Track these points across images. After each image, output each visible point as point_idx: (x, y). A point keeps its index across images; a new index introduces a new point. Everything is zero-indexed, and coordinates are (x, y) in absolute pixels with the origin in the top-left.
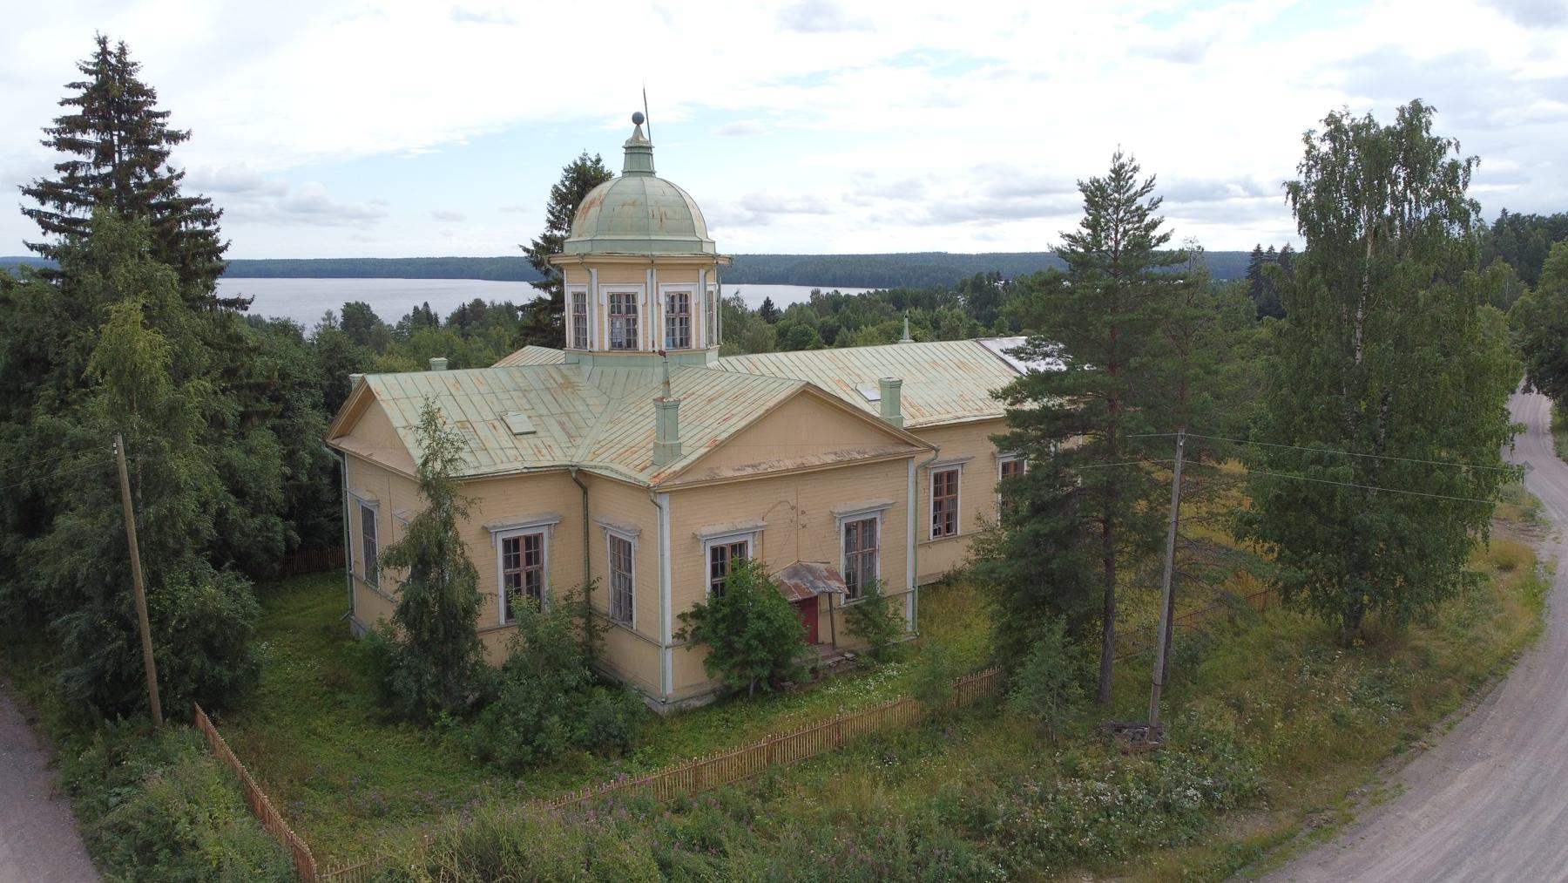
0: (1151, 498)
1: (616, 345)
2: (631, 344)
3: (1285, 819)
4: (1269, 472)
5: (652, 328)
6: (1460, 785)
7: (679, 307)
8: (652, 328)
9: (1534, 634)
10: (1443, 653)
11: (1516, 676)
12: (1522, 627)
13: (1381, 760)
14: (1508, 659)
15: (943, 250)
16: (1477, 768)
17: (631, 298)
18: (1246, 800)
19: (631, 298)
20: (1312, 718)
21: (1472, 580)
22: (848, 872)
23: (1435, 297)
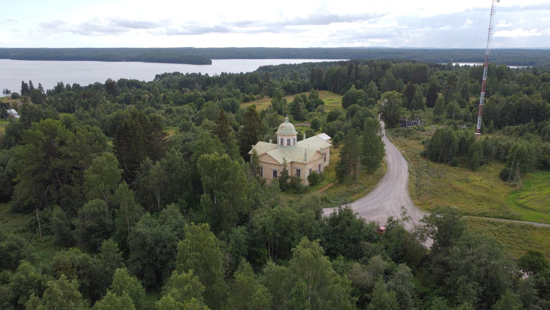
0: (295, 277)
1: (288, 145)
2: (290, 145)
3: (370, 189)
4: (44, 165)
5: (285, 143)
6: (382, 185)
7: (289, 140)
8: (285, 143)
9: (387, 171)
10: (378, 174)
11: (385, 175)
12: (386, 170)
13: (376, 184)
14: (384, 174)
15: (192, 46)
16: (383, 184)
17: (283, 139)
18: (367, 188)
19: (283, 139)
20: (369, 181)
21: (381, 166)
22: (349, 134)
23: (296, 271)
